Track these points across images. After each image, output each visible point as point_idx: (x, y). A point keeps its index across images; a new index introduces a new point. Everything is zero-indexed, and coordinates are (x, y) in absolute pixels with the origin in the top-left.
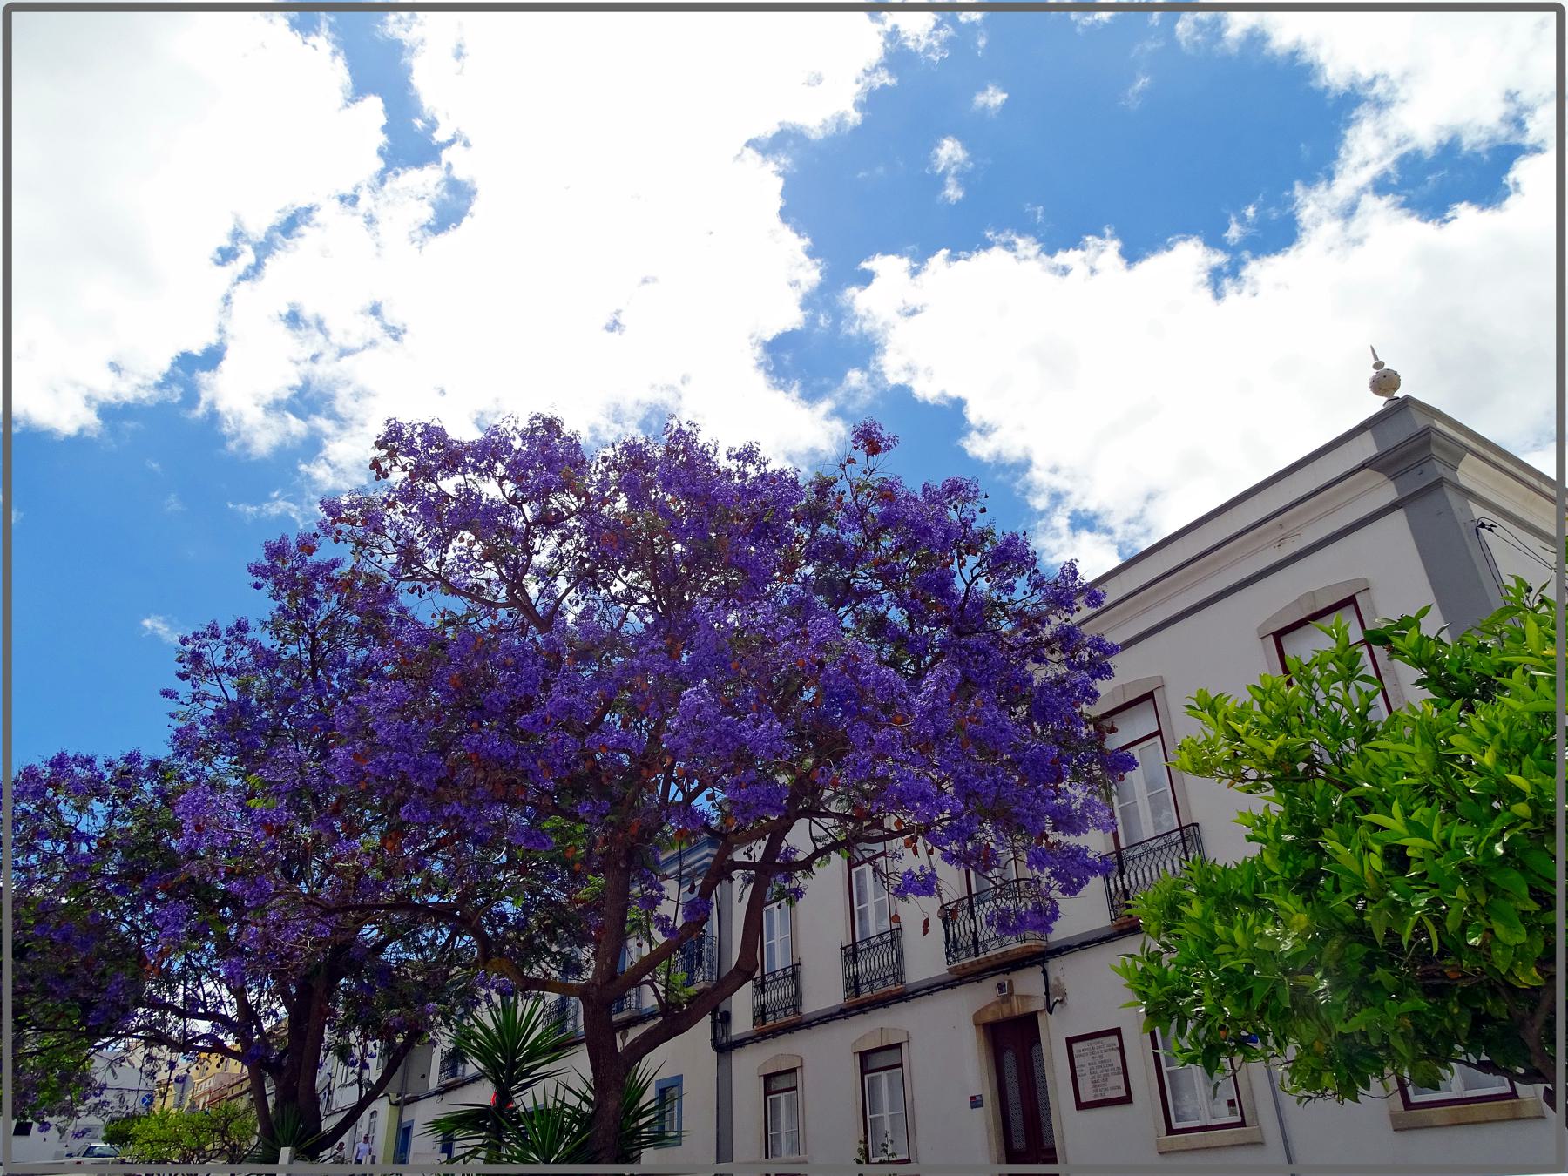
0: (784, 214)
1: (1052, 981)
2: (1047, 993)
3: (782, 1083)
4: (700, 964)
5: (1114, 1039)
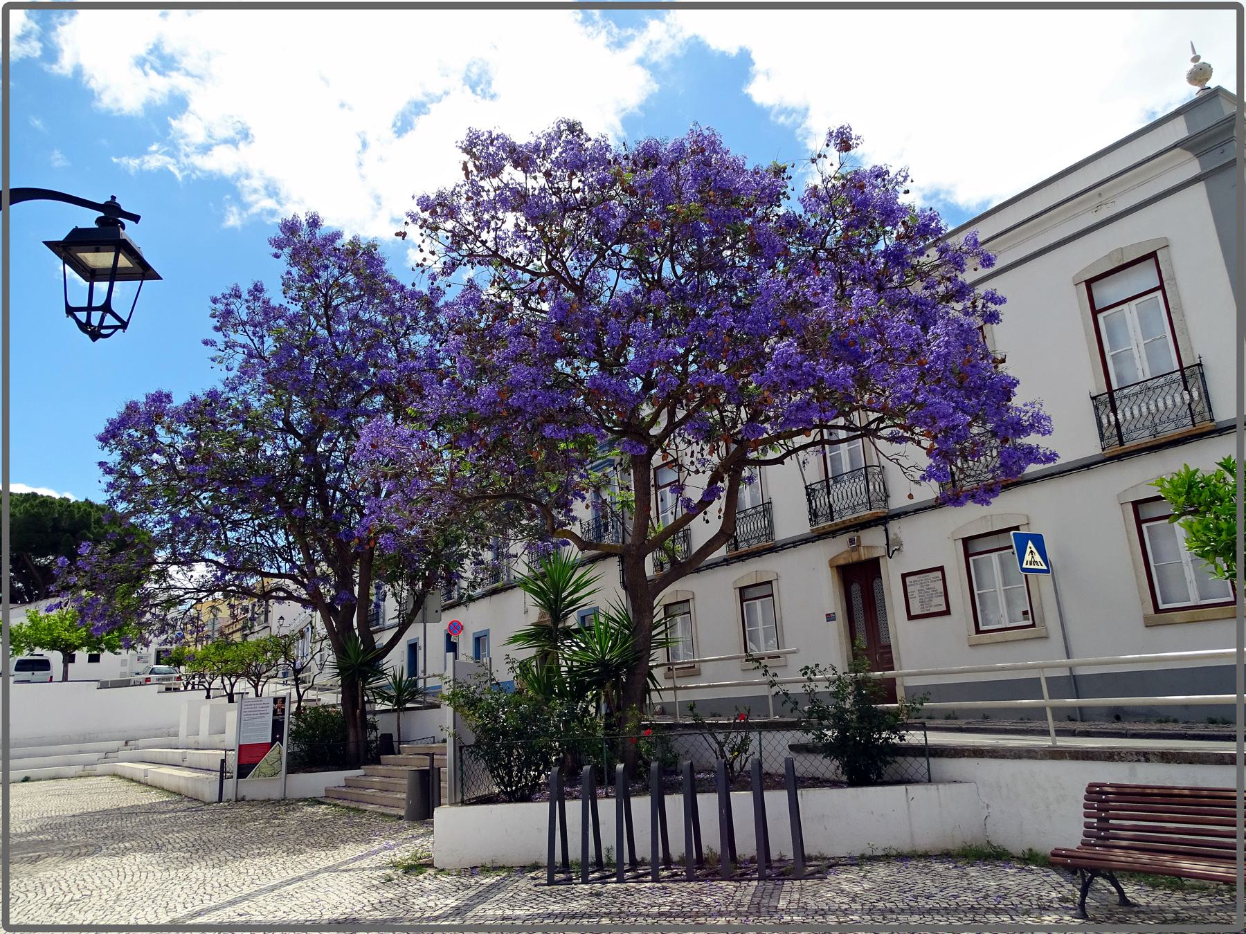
1: (891, 536)
2: (887, 544)
3: (675, 609)
4: (606, 530)
5: (939, 574)
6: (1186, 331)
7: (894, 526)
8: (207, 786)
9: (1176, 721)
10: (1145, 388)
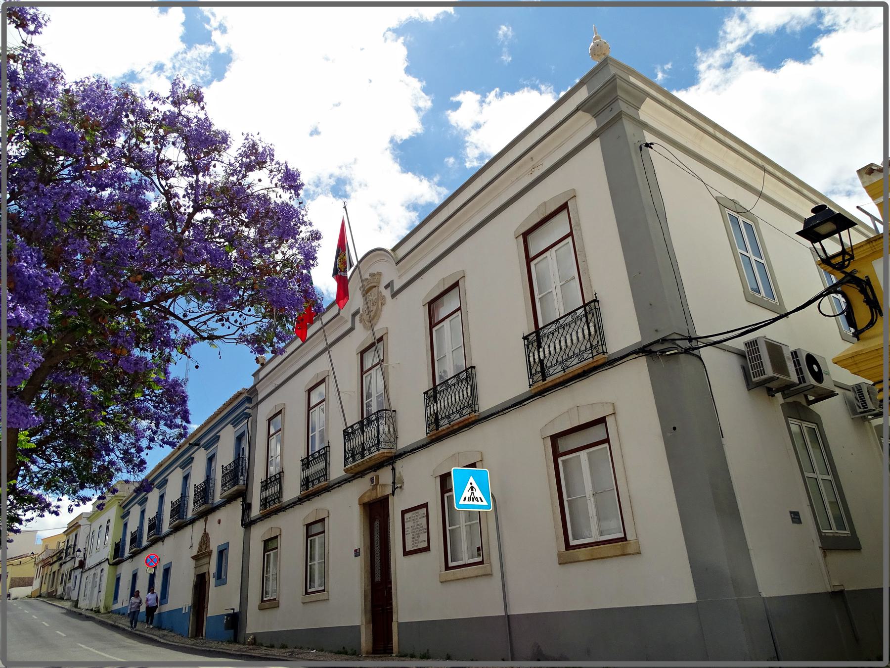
0: (408, 71)
1: (397, 475)
6: (587, 269)
7: (399, 464)
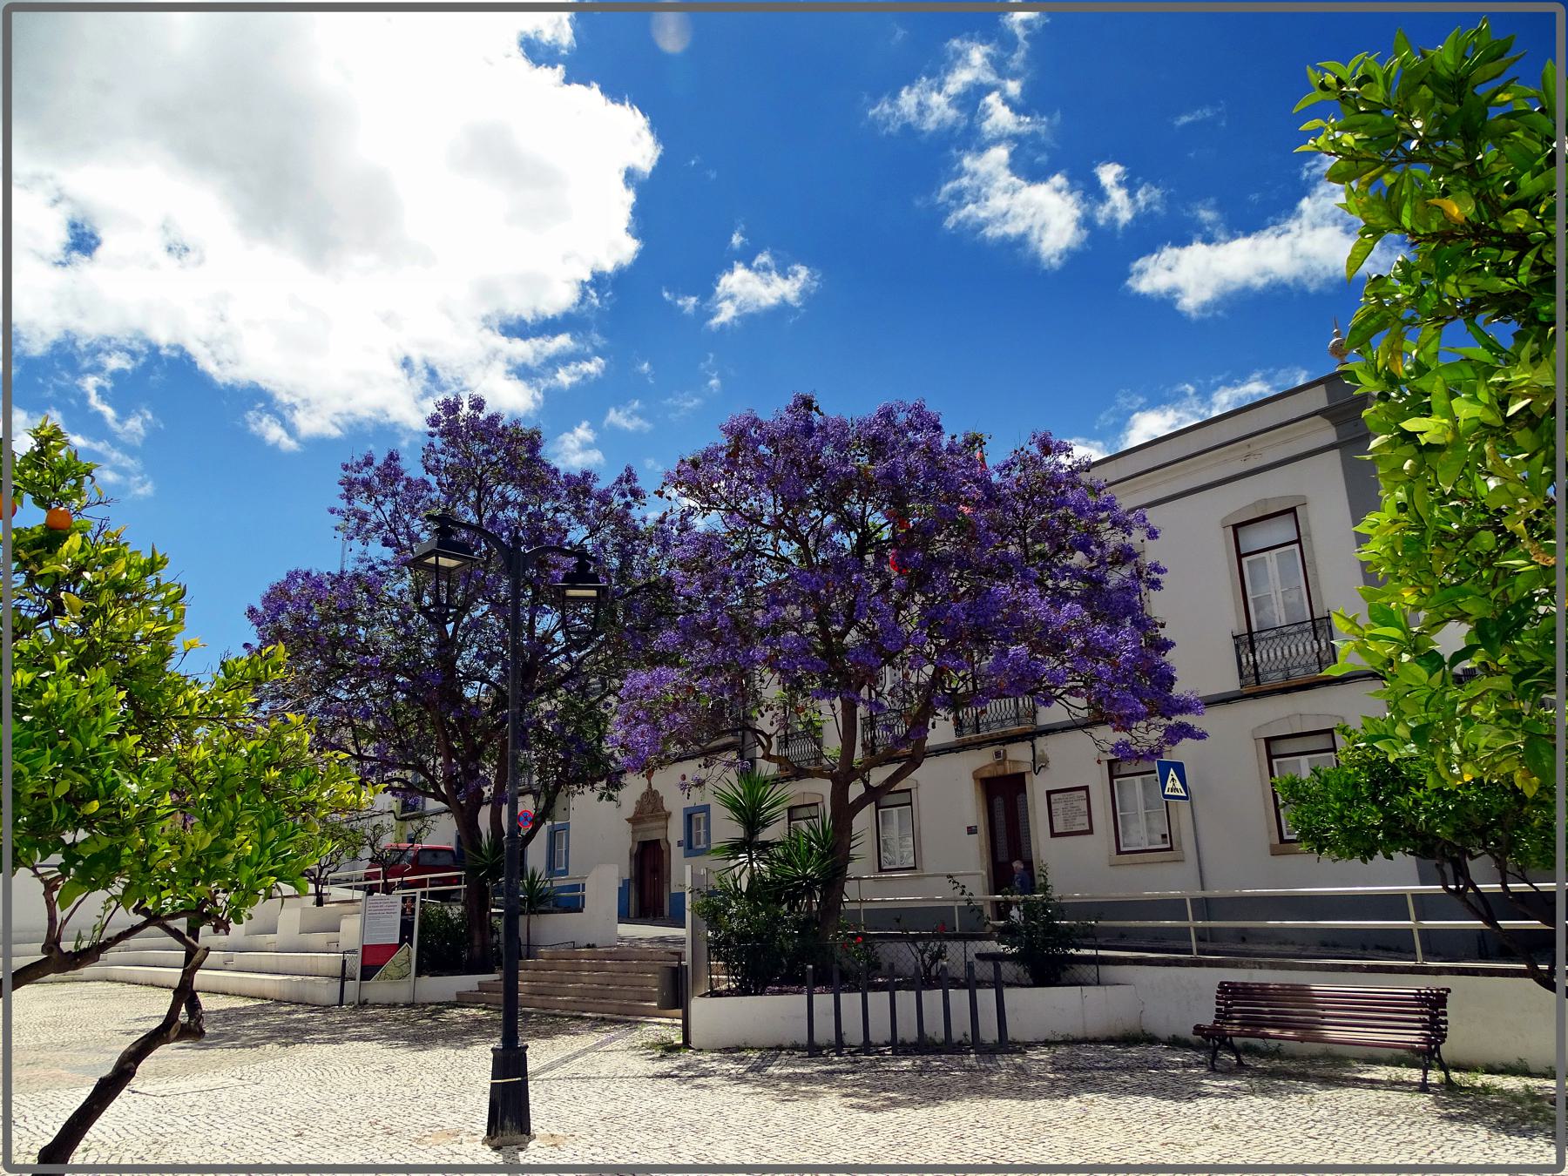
1: (1038, 752)
5: (1083, 793)
7: (1041, 742)
8: (327, 991)
9: (1293, 943)
10: (1280, 633)
